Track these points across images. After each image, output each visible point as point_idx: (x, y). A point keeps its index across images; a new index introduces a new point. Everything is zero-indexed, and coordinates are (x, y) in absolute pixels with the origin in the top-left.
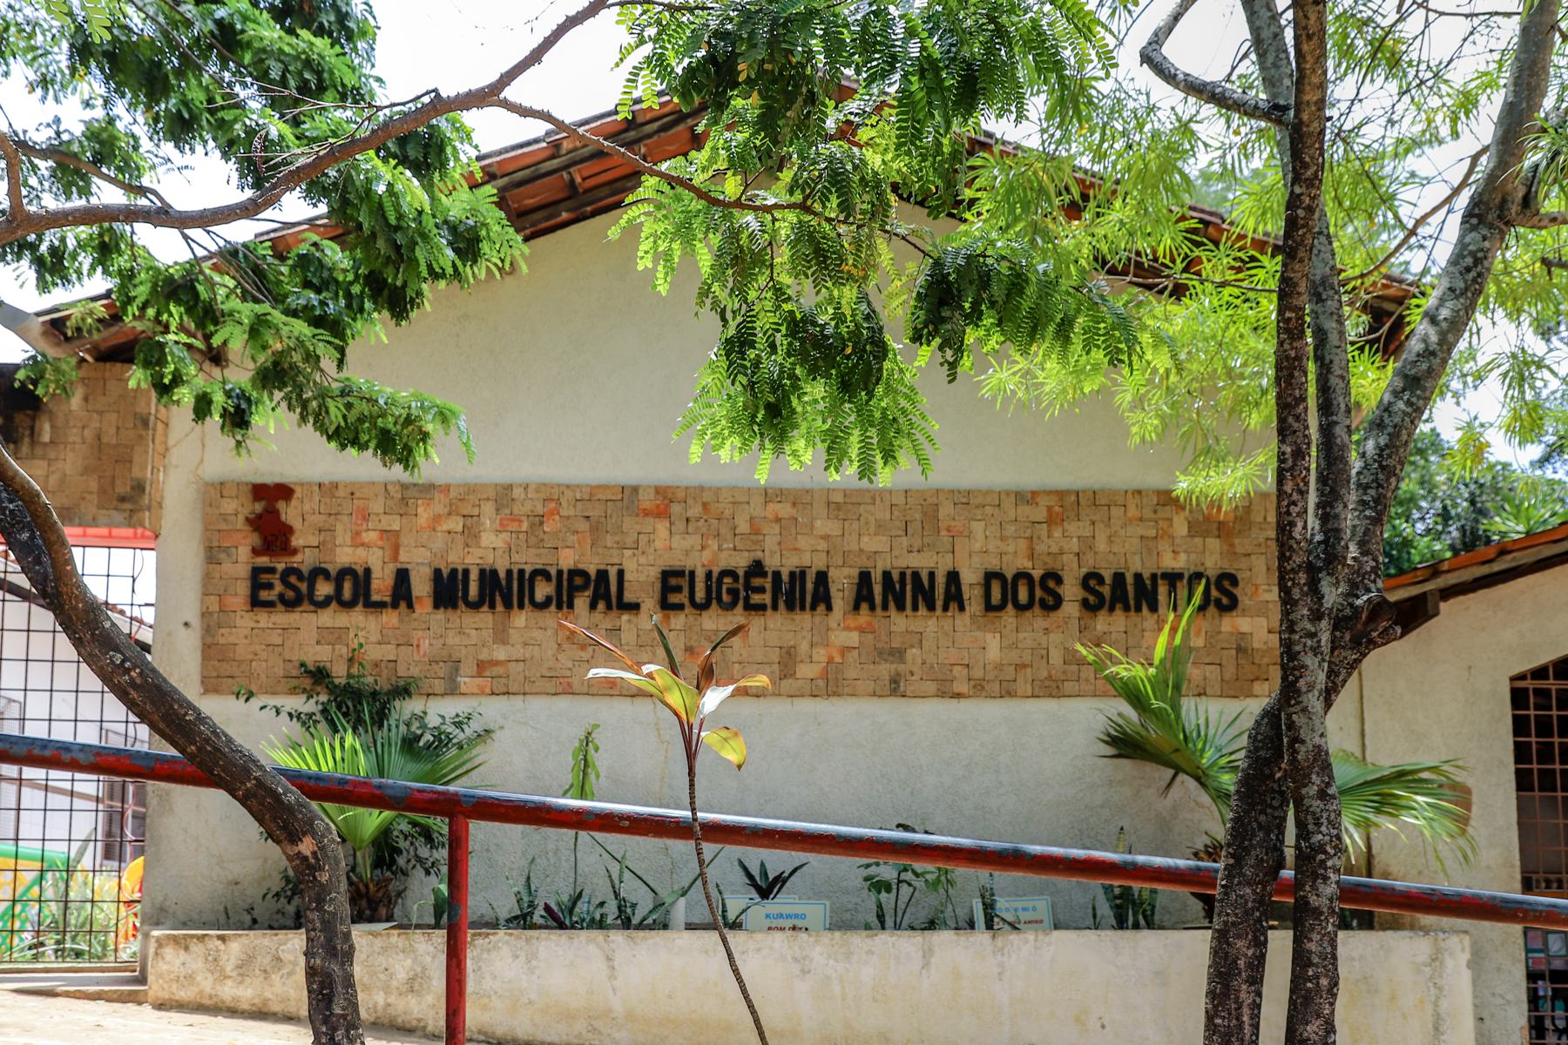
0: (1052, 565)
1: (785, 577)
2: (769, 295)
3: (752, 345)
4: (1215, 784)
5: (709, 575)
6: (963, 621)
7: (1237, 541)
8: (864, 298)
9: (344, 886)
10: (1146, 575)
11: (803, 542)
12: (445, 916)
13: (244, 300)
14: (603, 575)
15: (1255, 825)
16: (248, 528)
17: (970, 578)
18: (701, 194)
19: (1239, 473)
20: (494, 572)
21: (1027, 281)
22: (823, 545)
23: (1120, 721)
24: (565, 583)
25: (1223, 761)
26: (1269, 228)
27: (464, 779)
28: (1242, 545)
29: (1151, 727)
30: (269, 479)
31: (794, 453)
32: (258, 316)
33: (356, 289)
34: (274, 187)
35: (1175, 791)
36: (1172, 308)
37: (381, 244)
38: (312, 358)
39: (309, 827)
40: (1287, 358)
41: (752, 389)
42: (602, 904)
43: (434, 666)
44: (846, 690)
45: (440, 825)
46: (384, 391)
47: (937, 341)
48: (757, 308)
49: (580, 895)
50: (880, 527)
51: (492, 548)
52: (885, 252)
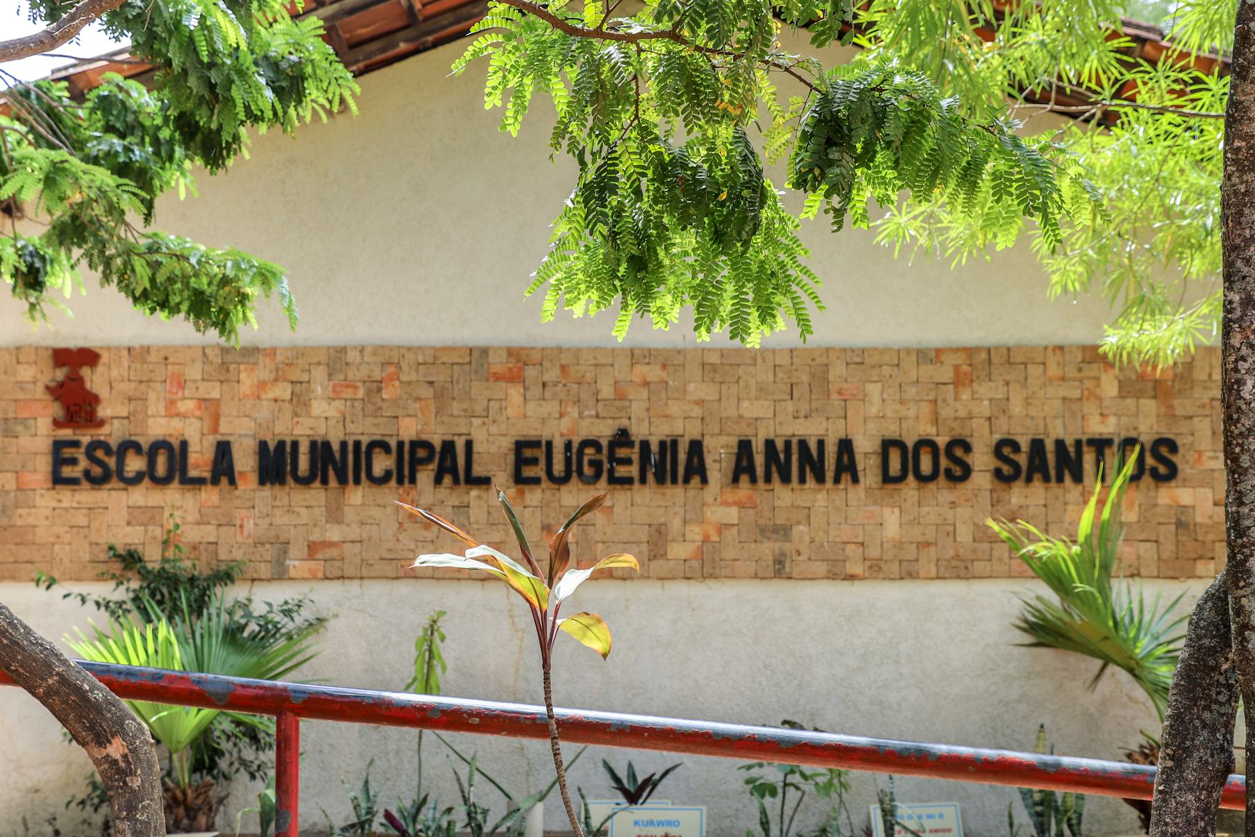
0: (959, 431)
1: (654, 448)
2: (635, 134)
3: (613, 191)
4: (1151, 677)
5: (568, 446)
6: (856, 494)
7: (1176, 402)
8: (741, 139)
9: (158, 792)
10: (1069, 441)
11: (675, 408)
12: (273, 825)
13: (37, 145)
14: (449, 446)
15: (1197, 723)
16: (48, 397)
17: (865, 446)
18: (556, 22)
19: (1178, 327)
20: (327, 445)
21: (929, 118)
22: (697, 411)
23: (1040, 606)
24: (406, 456)
25: (1160, 651)
26: (1217, 44)
27: (294, 672)
28: (1181, 406)
29: (1075, 613)
30: (72, 343)
31: (660, 311)
32: (54, 164)
33: (165, 134)
34: (73, 18)
35: (1105, 684)
36: (1100, 139)
37: (192, 82)
38: (114, 210)
39: (118, 726)
40: (1236, 193)
41: (614, 240)
42: (449, 810)
43: (260, 548)
44: (724, 572)
45: (267, 724)
46: (198, 248)
47: (824, 187)
48: (619, 150)
49: (424, 800)
50: (762, 390)
51: (325, 418)
52: (765, 84)
